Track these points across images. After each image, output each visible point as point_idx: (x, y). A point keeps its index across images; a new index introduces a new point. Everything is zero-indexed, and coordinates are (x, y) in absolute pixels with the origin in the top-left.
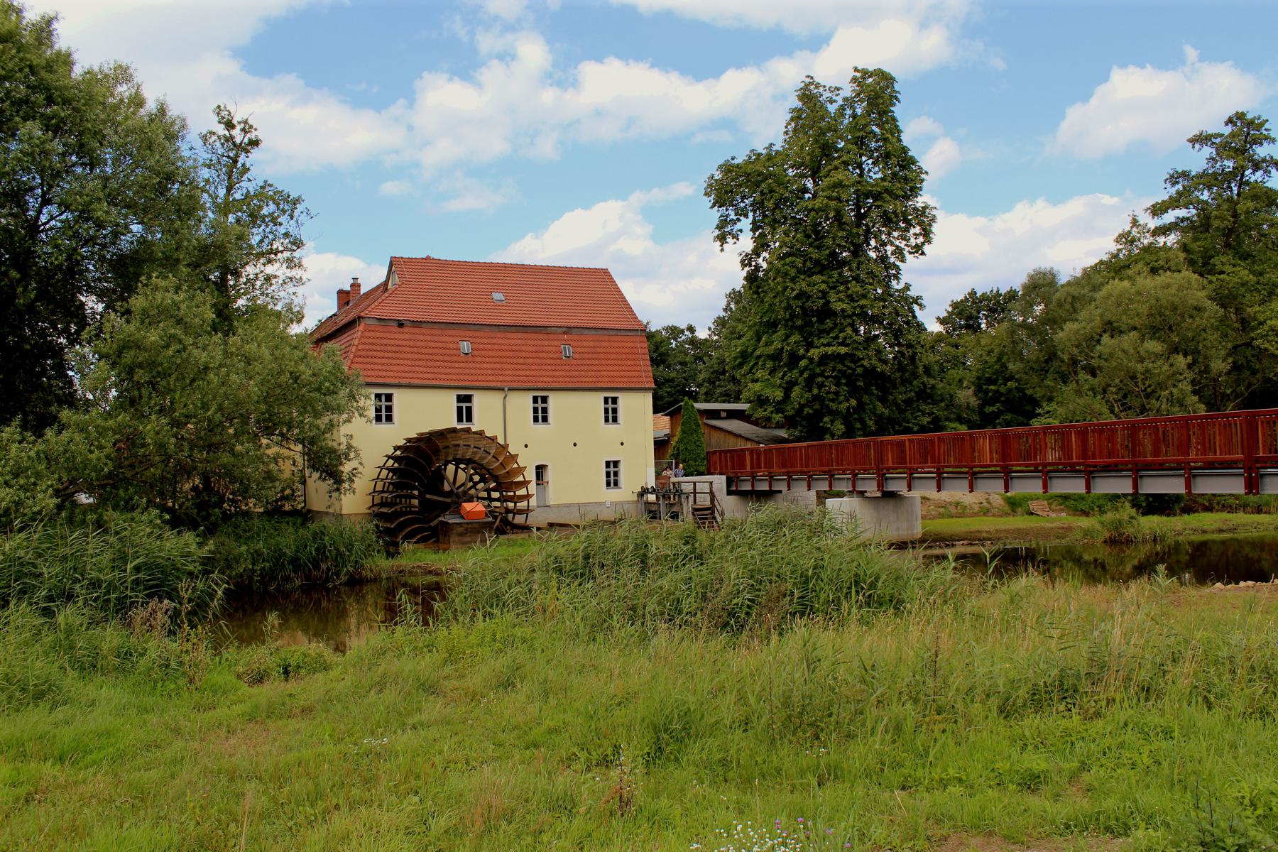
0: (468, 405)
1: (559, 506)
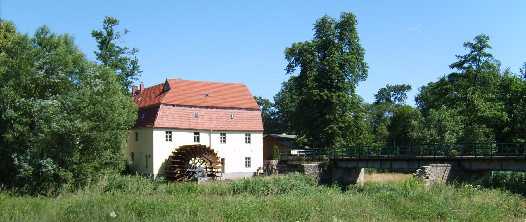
0: (198, 136)
1: (229, 173)
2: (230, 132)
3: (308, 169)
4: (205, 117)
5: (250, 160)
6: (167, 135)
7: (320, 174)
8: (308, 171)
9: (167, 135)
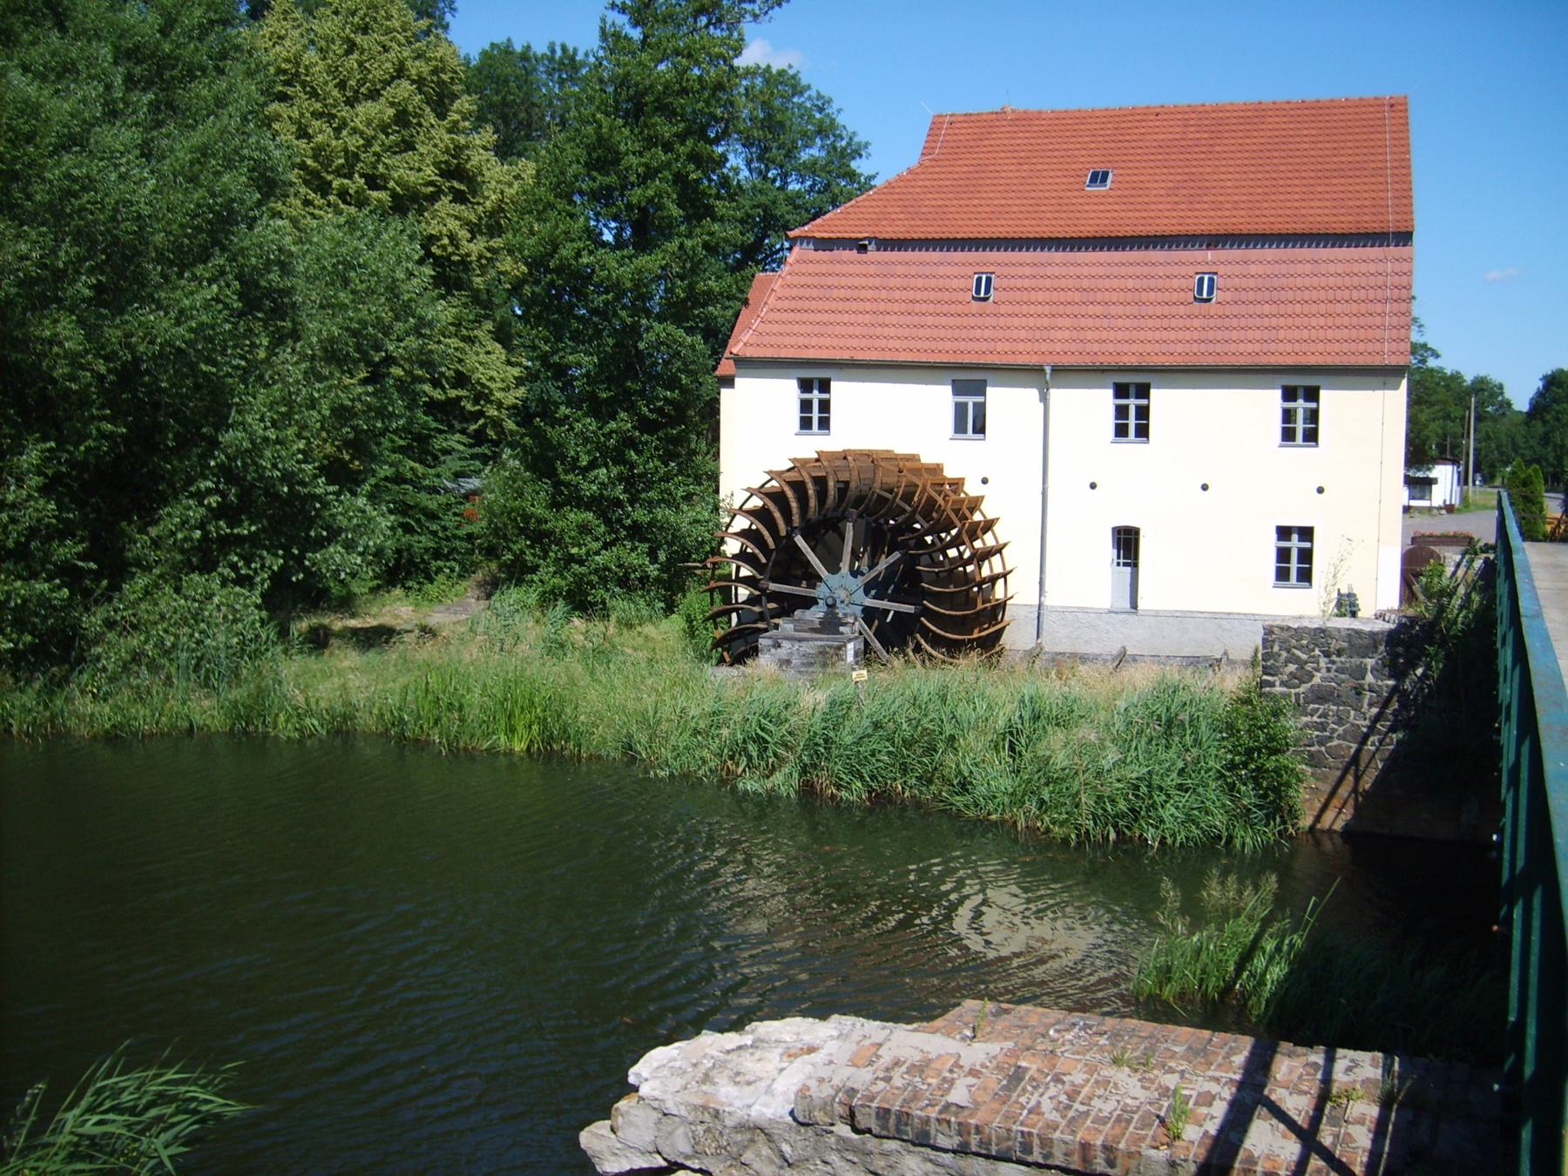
0: (980, 399)
1: (1157, 614)
2: (1181, 376)
3: (1293, 659)
4: (1033, 296)
5: (1311, 541)
6: (807, 396)
7: (1404, 705)
8: (1292, 667)
9: (807, 396)
